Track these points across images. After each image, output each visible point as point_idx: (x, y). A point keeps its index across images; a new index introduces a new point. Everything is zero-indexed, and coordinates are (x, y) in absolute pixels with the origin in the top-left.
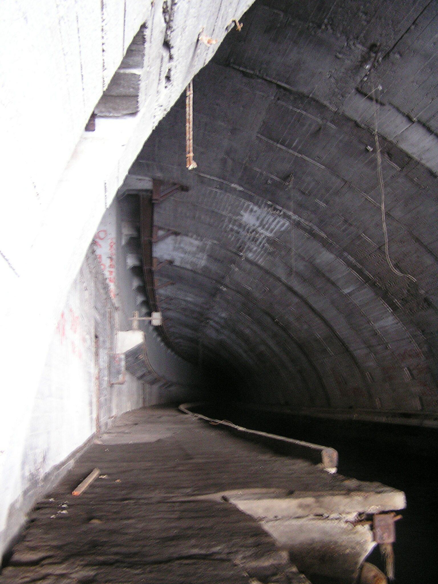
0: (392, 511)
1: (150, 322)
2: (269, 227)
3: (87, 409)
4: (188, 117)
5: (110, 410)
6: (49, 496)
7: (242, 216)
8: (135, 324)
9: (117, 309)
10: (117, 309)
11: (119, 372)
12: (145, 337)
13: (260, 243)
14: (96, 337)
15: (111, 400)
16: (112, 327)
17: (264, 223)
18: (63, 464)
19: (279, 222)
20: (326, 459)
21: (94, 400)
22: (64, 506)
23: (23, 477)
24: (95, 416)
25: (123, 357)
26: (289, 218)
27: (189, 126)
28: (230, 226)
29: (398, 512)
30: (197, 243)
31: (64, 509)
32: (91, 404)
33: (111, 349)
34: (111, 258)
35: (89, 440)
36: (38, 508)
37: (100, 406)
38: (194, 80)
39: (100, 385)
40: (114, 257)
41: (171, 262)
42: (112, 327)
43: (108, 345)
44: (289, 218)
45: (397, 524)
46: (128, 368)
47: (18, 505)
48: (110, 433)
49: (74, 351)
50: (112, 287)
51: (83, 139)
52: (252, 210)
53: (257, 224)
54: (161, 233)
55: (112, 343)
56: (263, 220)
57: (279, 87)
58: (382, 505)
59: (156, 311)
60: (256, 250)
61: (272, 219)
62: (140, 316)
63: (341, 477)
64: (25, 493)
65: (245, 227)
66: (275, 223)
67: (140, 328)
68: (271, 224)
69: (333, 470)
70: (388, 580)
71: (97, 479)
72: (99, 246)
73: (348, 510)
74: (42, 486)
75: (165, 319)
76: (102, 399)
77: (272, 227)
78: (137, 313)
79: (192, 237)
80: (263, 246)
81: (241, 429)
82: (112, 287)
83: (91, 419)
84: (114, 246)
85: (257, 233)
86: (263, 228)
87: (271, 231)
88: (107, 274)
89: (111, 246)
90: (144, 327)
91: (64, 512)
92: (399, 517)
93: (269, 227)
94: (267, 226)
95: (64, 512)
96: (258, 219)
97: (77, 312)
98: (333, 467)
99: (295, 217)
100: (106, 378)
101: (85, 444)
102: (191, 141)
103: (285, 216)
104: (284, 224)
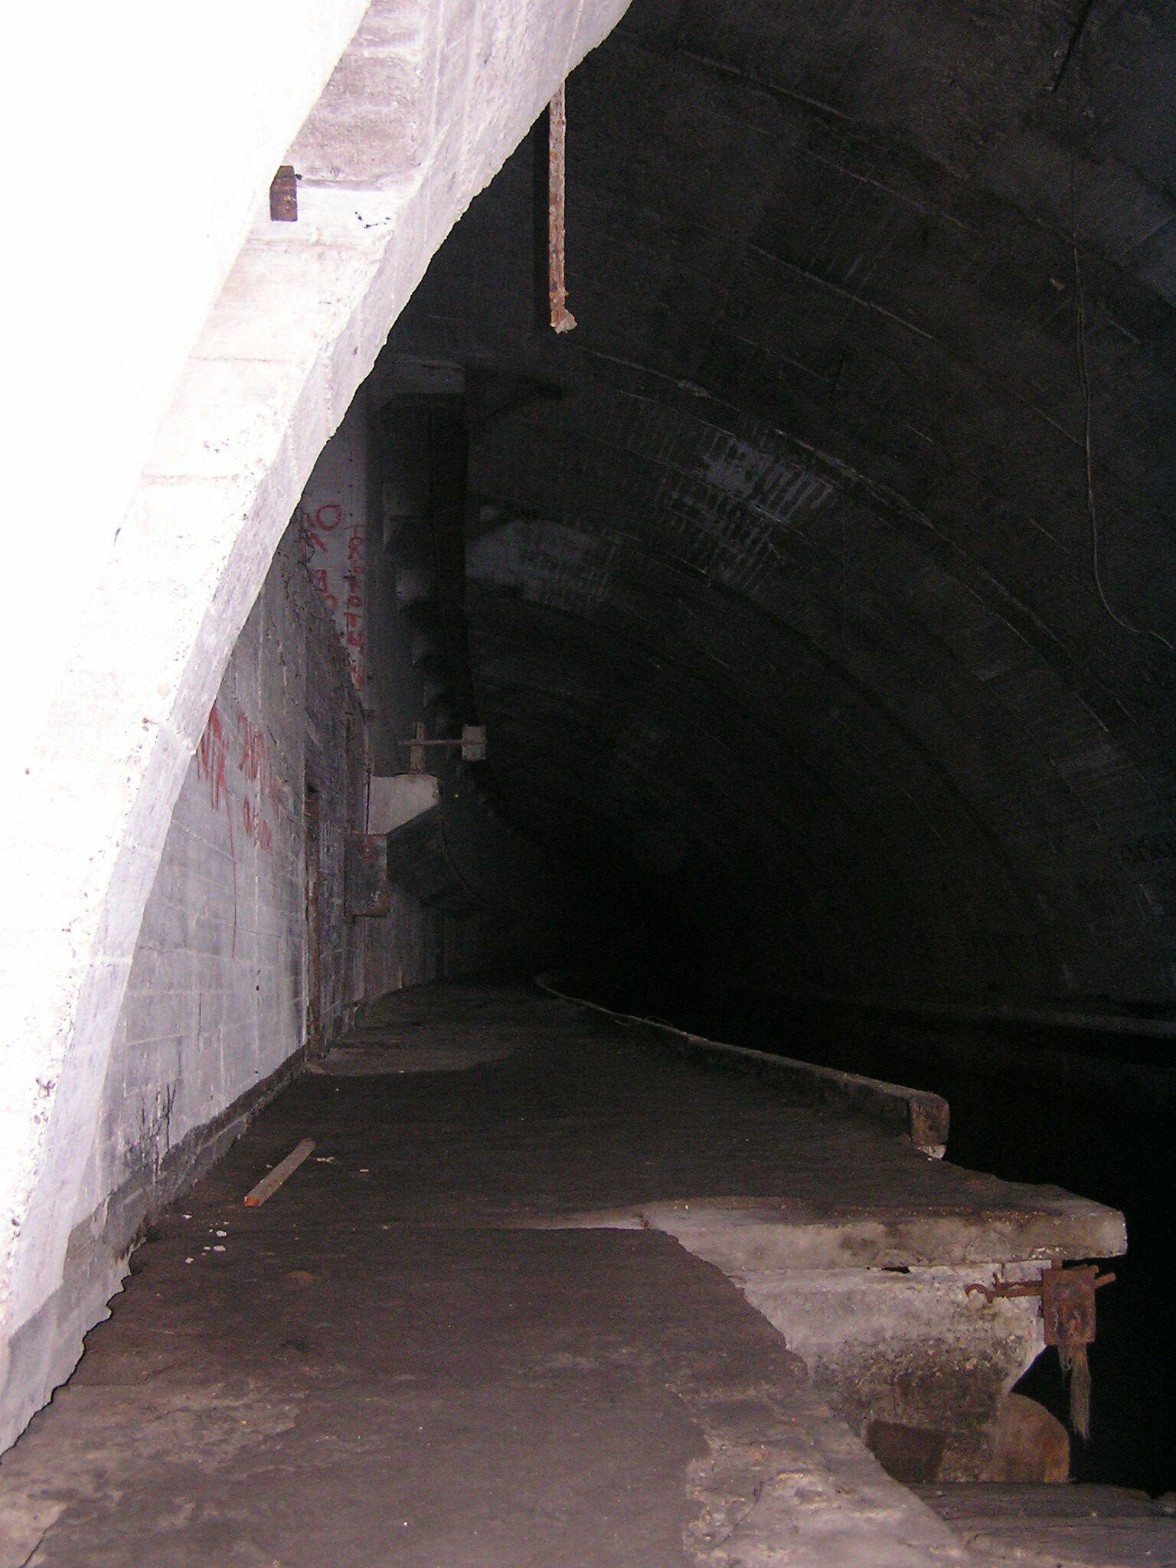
0: (1090, 1262)
1: (458, 751)
2: (779, 498)
3: (286, 980)
4: (552, 189)
5: (348, 987)
6: (177, 1206)
7: (707, 467)
8: (417, 756)
9: (367, 716)
10: (367, 716)
11: (371, 886)
12: (443, 791)
13: (755, 542)
14: (311, 789)
15: (350, 959)
16: (355, 764)
17: (766, 488)
18: (218, 1123)
19: (806, 484)
20: (920, 1124)
21: (305, 958)
22: (221, 1234)
23: (109, 1155)
24: (305, 1000)
25: (383, 843)
26: (833, 473)
27: (557, 213)
28: (675, 495)
29: (1105, 1265)
30: (583, 539)
31: (220, 1241)
32: (295, 968)
33: (352, 823)
34: (352, 580)
35: (290, 1064)
36: (151, 1235)
37: (319, 979)
38: (574, 81)
39: (321, 917)
40: (361, 577)
41: (514, 592)
42: (355, 764)
43: (343, 811)
44: (833, 473)
45: (1102, 1295)
46: (395, 875)
47: (96, 1230)
48: (347, 1046)
49: (249, 827)
50: (355, 655)
51: (252, 245)
52: (733, 453)
53: (748, 490)
54: (488, 513)
55: (353, 806)
56: (763, 479)
57: (815, 111)
58: (1065, 1247)
59: (474, 723)
60: (744, 561)
61: (788, 476)
62: (429, 735)
63: (958, 1169)
64: (115, 1197)
65: (714, 498)
66: (792, 490)
67: (429, 769)
68: (784, 491)
69: (940, 1152)
70: (1075, 1438)
71: (306, 1166)
72: (317, 547)
73: (973, 1257)
74: (163, 1182)
75: (493, 741)
76: (326, 955)
77: (788, 497)
78: (420, 728)
79: (571, 524)
80: (764, 549)
81: (694, 1038)
82: (355, 655)
83: (297, 1007)
84: (361, 549)
85: (745, 513)
86: (763, 501)
87: (784, 512)
88: (341, 622)
89: (353, 548)
90: (440, 764)
91: (220, 1248)
92: (1111, 1277)
93: (779, 498)
94: (772, 497)
95: (220, 1248)
96: (749, 476)
97: (258, 723)
98: (941, 1144)
99: (851, 473)
100: (338, 901)
101: (279, 1074)
102: (562, 256)
103: (823, 469)
104: (818, 493)
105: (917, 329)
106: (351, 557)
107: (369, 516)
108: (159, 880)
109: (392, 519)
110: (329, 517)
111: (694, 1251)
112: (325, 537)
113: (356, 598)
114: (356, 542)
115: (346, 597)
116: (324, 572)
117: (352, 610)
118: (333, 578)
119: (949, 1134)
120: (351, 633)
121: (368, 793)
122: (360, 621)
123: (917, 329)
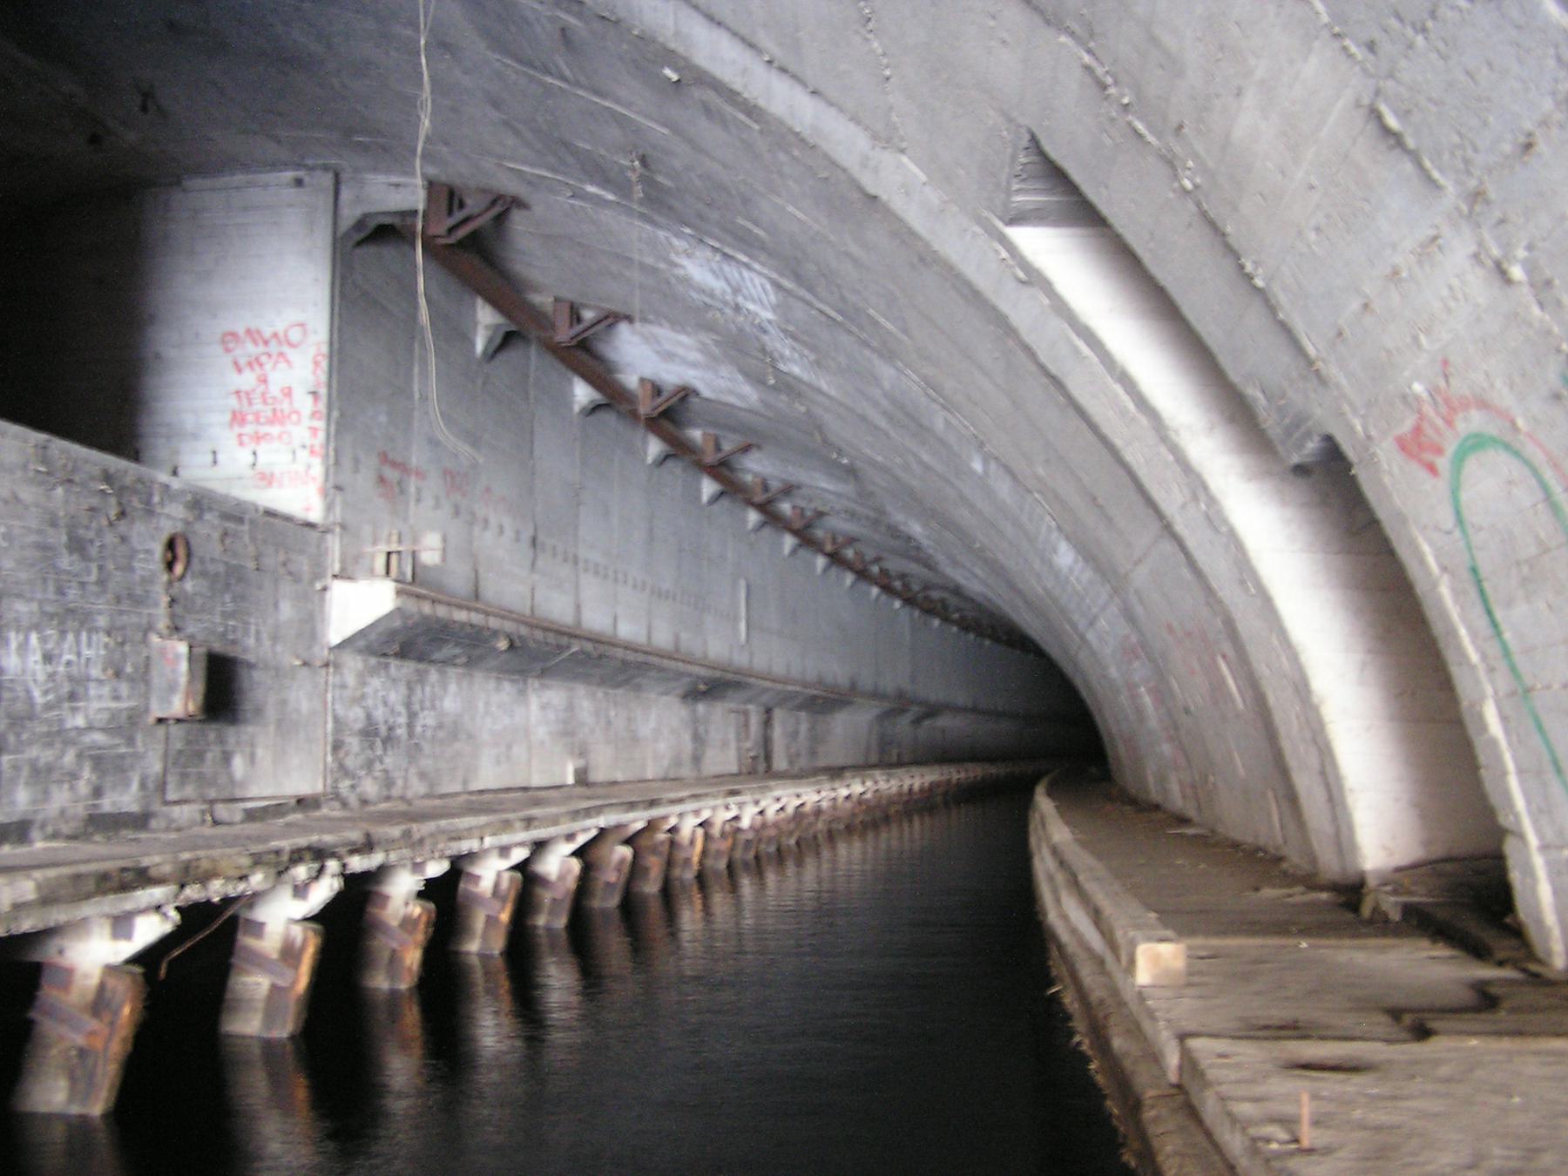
89: (316, 364)
109: (487, 327)
122: (321, 436)
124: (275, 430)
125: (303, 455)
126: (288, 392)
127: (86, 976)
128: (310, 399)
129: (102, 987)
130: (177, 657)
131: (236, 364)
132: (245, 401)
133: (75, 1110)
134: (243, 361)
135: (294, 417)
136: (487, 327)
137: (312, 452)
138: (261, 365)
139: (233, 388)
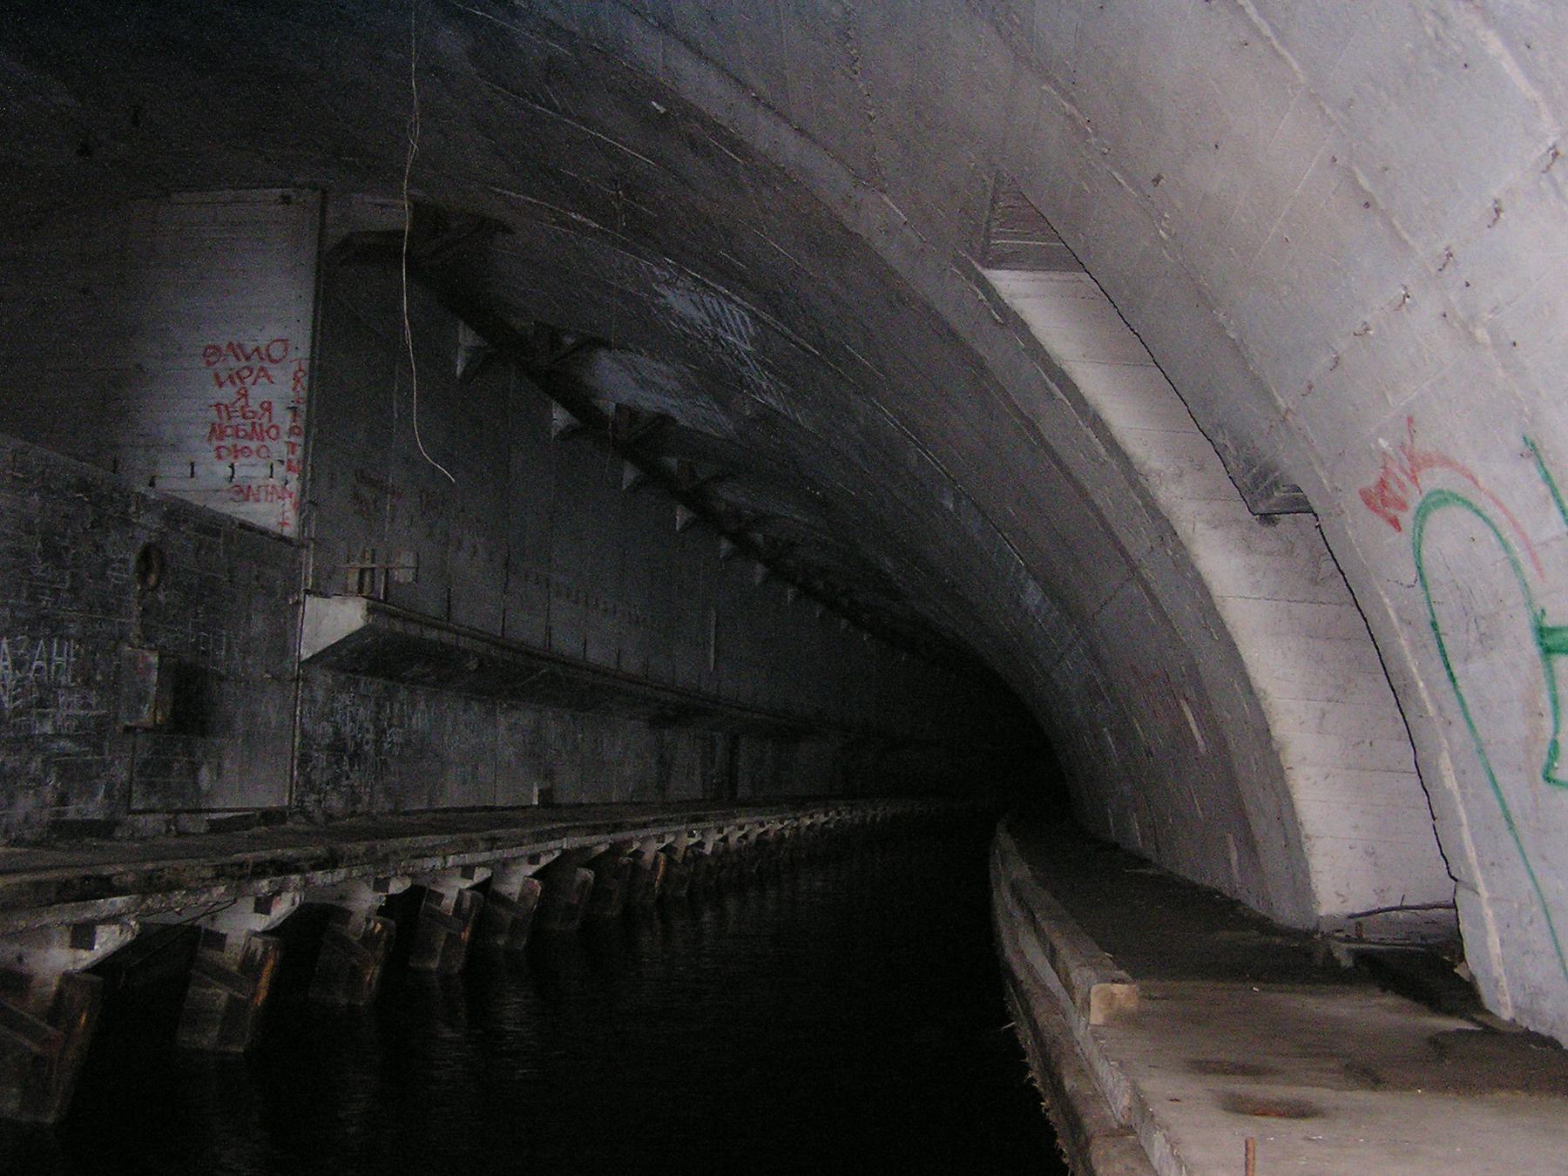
84: (305, 381)
105: (727, 152)
106: (294, 389)
107: (505, 226)
108: (1407, 1086)
110: (277, 352)
111: (280, 899)
112: (274, 371)
113: (296, 427)
114: (300, 374)
115: (288, 427)
116: (270, 403)
117: (292, 439)
118: (278, 408)
119: (389, 884)
120: (290, 461)
121: (303, 614)
122: (299, 451)
123: (727, 152)
124: (253, 445)
125: (280, 470)
126: (267, 407)
127: (45, 983)
128: (289, 415)
129: (60, 993)
130: (149, 667)
131: (217, 376)
132: (224, 415)
133: (26, 1118)
134: (224, 376)
135: (273, 432)
136: (469, 350)
137: (289, 469)
138: (242, 379)
139: (212, 402)
